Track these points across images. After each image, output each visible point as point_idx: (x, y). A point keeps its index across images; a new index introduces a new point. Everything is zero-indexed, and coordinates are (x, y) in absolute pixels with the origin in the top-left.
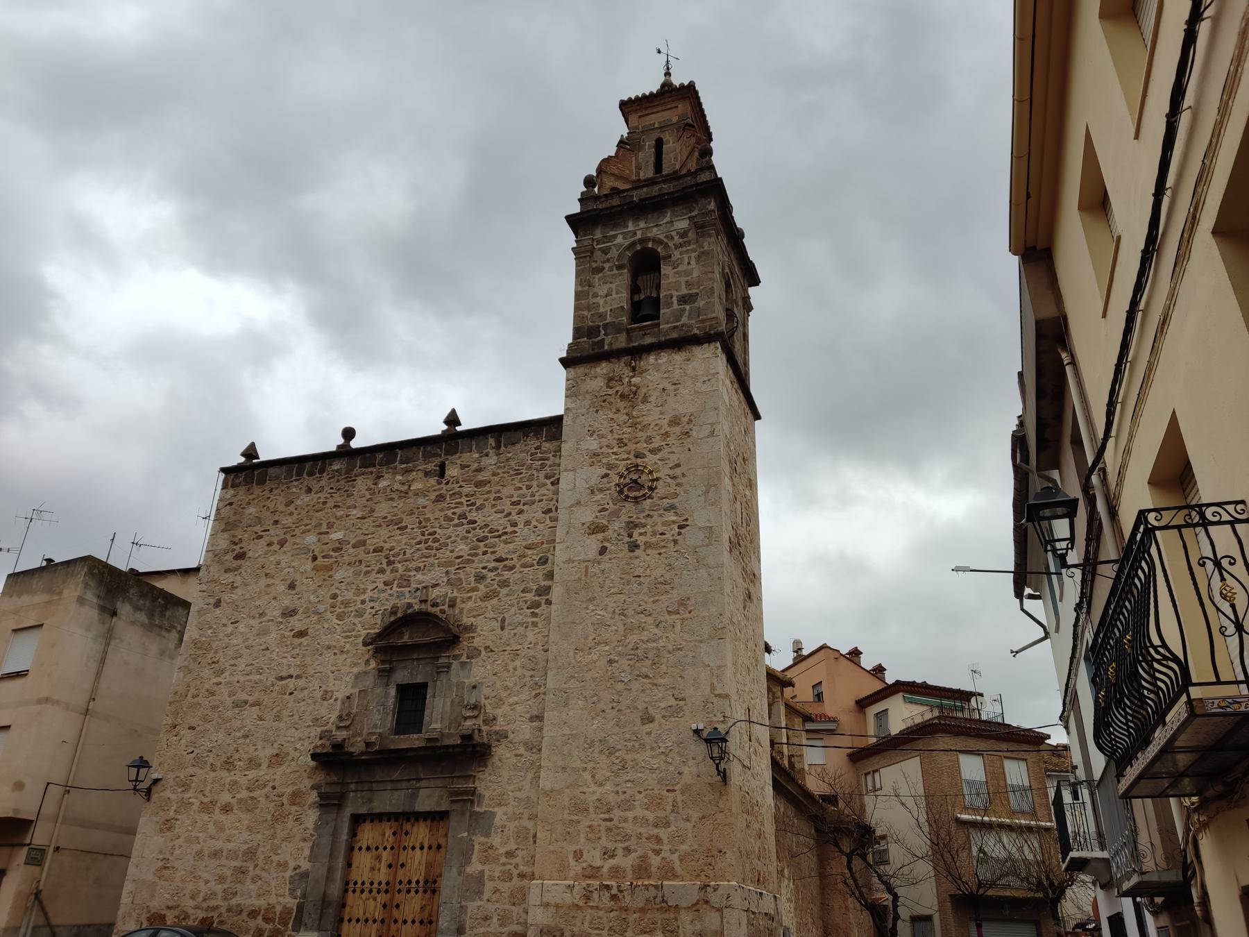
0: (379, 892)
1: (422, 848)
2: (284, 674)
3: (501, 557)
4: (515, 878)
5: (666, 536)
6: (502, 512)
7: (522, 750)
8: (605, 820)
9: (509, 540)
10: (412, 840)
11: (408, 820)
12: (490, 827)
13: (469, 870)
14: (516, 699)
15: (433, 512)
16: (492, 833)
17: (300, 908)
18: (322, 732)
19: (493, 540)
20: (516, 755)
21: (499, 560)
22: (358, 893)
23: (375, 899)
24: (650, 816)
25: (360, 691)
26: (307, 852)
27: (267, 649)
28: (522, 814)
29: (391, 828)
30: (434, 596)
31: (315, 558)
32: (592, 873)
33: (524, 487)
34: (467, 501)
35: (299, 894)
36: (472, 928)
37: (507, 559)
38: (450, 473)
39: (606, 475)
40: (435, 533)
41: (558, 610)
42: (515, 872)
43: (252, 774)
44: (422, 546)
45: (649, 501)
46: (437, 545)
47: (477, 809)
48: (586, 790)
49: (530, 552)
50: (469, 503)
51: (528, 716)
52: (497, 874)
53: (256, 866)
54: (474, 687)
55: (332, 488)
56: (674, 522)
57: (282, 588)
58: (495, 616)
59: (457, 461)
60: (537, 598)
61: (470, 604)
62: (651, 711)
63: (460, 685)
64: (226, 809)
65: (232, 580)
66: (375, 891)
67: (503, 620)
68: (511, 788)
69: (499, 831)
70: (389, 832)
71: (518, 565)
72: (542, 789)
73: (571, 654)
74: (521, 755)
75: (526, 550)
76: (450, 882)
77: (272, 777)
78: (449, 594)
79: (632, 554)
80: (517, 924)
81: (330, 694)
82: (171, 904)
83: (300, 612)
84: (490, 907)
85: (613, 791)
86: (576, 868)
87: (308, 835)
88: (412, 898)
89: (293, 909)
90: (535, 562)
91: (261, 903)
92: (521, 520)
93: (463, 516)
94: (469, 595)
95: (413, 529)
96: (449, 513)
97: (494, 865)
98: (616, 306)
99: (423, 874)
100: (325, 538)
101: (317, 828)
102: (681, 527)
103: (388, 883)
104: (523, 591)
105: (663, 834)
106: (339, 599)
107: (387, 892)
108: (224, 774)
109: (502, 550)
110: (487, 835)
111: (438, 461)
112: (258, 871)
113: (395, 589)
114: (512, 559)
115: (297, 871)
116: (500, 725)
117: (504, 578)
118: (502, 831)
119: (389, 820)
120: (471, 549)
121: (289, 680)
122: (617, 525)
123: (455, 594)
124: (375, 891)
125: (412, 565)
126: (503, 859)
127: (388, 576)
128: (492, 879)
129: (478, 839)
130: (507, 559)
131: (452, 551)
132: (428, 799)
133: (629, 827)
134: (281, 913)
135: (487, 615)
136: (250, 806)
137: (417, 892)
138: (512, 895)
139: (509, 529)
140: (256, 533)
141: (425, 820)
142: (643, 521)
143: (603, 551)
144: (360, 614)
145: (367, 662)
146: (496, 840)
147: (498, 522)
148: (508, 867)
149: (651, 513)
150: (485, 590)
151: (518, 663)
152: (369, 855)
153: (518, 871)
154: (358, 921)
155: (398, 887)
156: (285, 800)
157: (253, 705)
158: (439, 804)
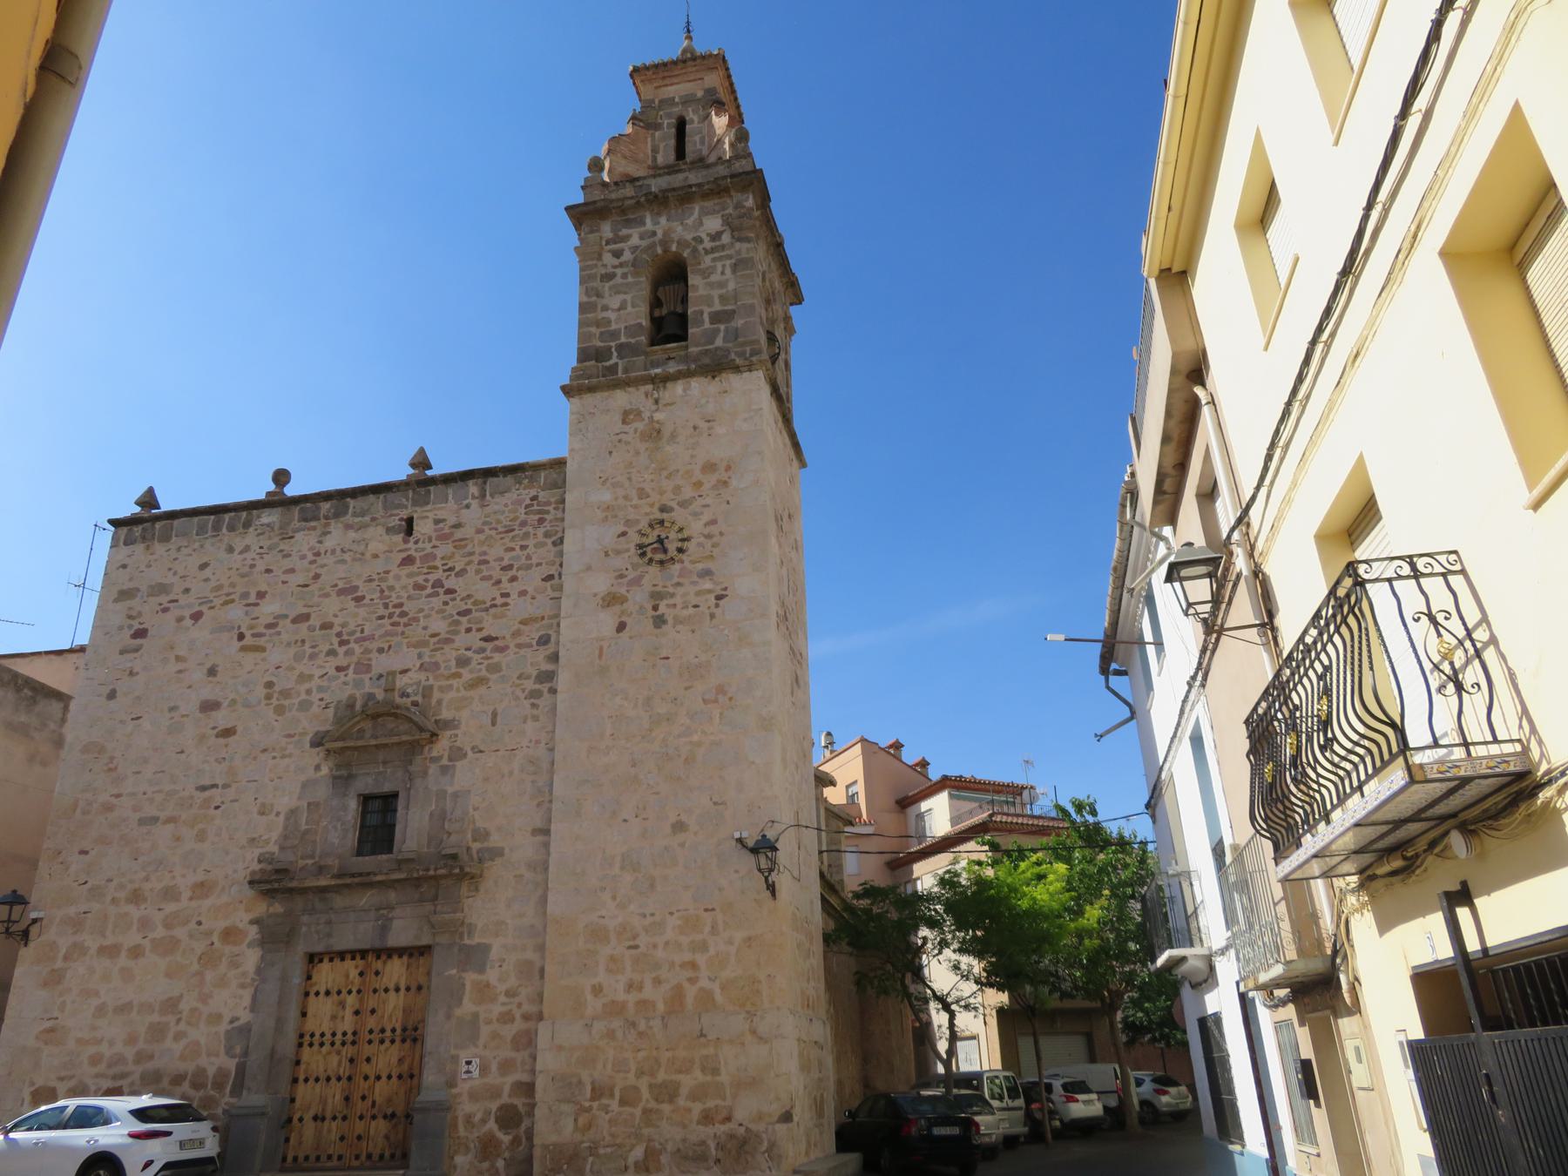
0: (343, 1044)
1: (397, 990)
5: (700, 609)
6: (489, 578)
8: (630, 947)
10: (384, 979)
11: (378, 958)
13: (458, 1012)
15: (397, 577)
21: (487, 639)
22: (316, 1047)
23: (338, 1053)
24: (685, 940)
26: (247, 1001)
27: (182, 752)
29: (356, 967)
31: (241, 637)
32: (615, 1009)
33: (518, 548)
38: (420, 529)
39: (624, 534)
40: (401, 605)
43: (171, 907)
44: (386, 621)
45: (677, 566)
46: (405, 620)
47: (467, 941)
48: (603, 913)
50: (446, 567)
53: (179, 1020)
55: (261, 548)
56: (710, 591)
57: (198, 675)
59: (428, 514)
61: (452, 694)
62: (684, 818)
63: (442, 794)
64: (136, 952)
65: (129, 665)
66: (338, 1043)
67: (495, 715)
70: (354, 973)
76: (436, 1029)
79: (658, 631)
82: (63, 1074)
83: (225, 704)
85: (639, 914)
86: (593, 1005)
88: (387, 1049)
90: (534, 643)
92: (514, 589)
93: (438, 584)
94: (450, 682)
96: (420, 579)
98: (632, 323)
99: (400, 1020)
101: (259, 971)
102: (719, 598)
103: (354, 1033)
104: (519, 677)
105: (701, 959)
107: (354, 1043)
108: (131, 908)
109: (491, 626)
110: (482, 970)
112: (182, 1026)
116: (495, 840)
119: (353, 958)
120: (450, 624)
122: (639, 597)
123: (431, 681)
124: (338, 1043)
125: (374, 645)
126: (502, 998)
127: (341, 660)
128: (489, 1022)
129: (470, 977)
131: (425, 628)
132: (403, 933)
133: (660, 953)
134: (214, 1077)
136: (168, 946)
137: (393, 1042)
139: (499, 601)
141: (400, 956)
142: (671, 590)
143: (621, 627)
144: (305, 706)
145: (318, 768)
146: (492, 975)
147: (484, 591)
149: (681, 580)
150: (470, 676)
152: (329, 1000)
154: (317, 1080)
155: (368, 1037)
156: (215, 938)
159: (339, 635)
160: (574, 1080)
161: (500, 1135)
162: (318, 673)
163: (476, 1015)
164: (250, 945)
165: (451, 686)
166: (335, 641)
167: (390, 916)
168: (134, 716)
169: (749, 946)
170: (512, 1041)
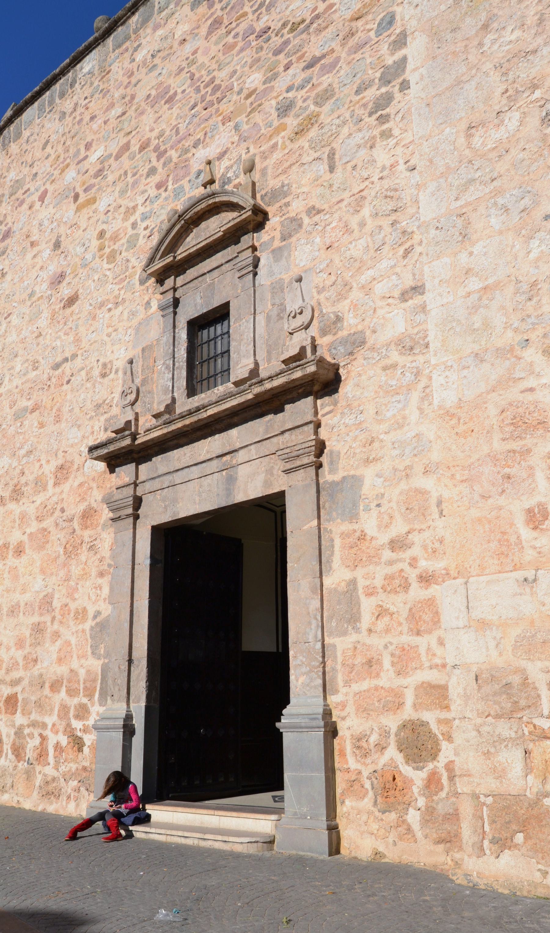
2: (59, 359)
3: (314, 57)
4: (415, 585)
7: (395, 356)
9: (324, 25)
12: (355, 505)
14: (370, 273)
16: (362, 513)
17: (105, 670)
18: (106, 420)
19: (297, 41)
20: (385, 369)
25: (143, 350)
26: (106, 591)
28: (410, 467)
30: (222, 171)
31: (76, 197)
34: (251, 7)
35: (102, 652)
36: (347, 683)
37: (324, 56)
41: (422, 78)
42: (412, 575)
48: (531, 382)
49: (360, 23)
51: (396, 294)
52: (378, 582)
54: (300, 280)
55: (86, 98)
58: (316, 155)
60: (384, 90)
67: (332, 156)
68: (384, 427)
69: (373, 505)
71: (343, 55)
72: (440, 407)
73: (462, 140)
74: (394, 366)
75: (354, 24)
77: (60, 497)
78: (244, 156)
80: (431, 668)
81: (109, 366)
84: (376, 641)
87: (106, 567)
89: (97, 674)
90: (372, 34)
91: (62, 670)
94: (273, 141)
95: (184, 91)
97: (371, 567)
100: (86, 165)
106: (108, 235)
110: (354, 517)
111: (137, 442)
112: (56, 626)
113: (170, 187)
114: (333, 51)
115: (98, 620)
117: (325, 85)
118: (378, 505)
121: (65, 364)
126: (387, 554)
128: (371, 592)
130: (324, 56)
135: (306, 159)
138: (412, 616)
140: (18, 200)
144: (132, 243)
148: (400, 566)
150: (295, 123)
151: (366, 212)
153: (417, 572)
156: (76, 524)
157: (33, 411)
158: (267, 483)
159: (157, 149)
160: (516, 680)
161: (407, 770)
162: (140, 200)
163: (353, 582)
164: (104, 526)
165: (274, 146)
166: (153, 157)
167: (234, 462)
168: (6, 315)
169: (55, 424)
170: (437, 743)
